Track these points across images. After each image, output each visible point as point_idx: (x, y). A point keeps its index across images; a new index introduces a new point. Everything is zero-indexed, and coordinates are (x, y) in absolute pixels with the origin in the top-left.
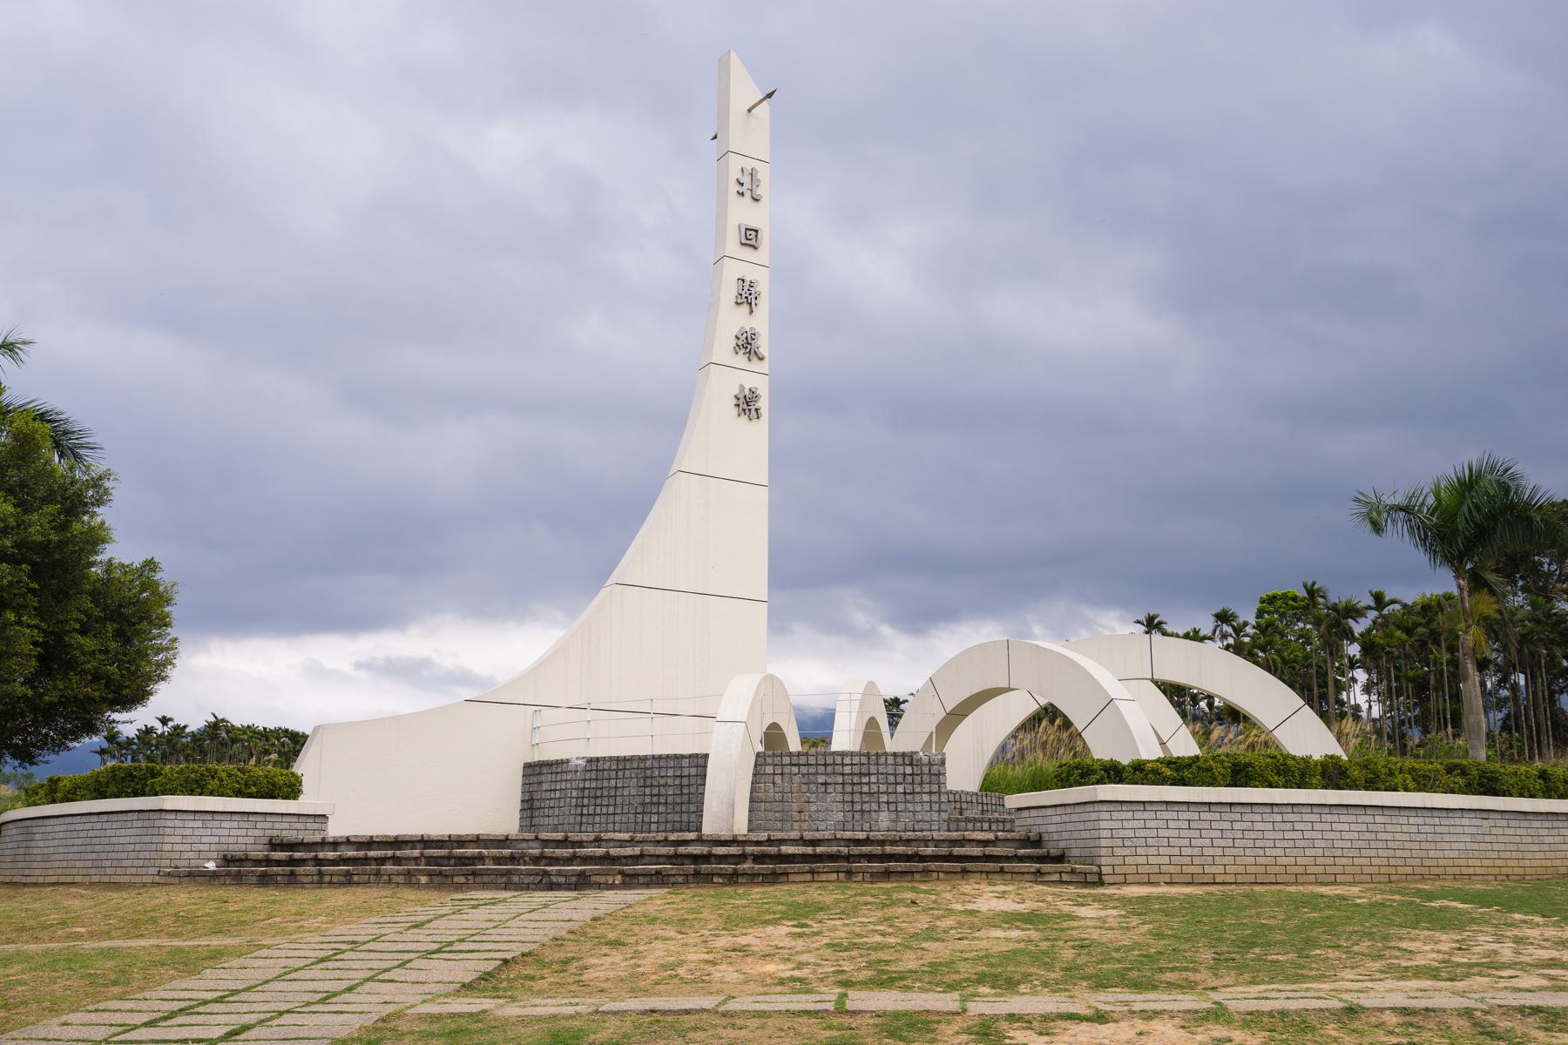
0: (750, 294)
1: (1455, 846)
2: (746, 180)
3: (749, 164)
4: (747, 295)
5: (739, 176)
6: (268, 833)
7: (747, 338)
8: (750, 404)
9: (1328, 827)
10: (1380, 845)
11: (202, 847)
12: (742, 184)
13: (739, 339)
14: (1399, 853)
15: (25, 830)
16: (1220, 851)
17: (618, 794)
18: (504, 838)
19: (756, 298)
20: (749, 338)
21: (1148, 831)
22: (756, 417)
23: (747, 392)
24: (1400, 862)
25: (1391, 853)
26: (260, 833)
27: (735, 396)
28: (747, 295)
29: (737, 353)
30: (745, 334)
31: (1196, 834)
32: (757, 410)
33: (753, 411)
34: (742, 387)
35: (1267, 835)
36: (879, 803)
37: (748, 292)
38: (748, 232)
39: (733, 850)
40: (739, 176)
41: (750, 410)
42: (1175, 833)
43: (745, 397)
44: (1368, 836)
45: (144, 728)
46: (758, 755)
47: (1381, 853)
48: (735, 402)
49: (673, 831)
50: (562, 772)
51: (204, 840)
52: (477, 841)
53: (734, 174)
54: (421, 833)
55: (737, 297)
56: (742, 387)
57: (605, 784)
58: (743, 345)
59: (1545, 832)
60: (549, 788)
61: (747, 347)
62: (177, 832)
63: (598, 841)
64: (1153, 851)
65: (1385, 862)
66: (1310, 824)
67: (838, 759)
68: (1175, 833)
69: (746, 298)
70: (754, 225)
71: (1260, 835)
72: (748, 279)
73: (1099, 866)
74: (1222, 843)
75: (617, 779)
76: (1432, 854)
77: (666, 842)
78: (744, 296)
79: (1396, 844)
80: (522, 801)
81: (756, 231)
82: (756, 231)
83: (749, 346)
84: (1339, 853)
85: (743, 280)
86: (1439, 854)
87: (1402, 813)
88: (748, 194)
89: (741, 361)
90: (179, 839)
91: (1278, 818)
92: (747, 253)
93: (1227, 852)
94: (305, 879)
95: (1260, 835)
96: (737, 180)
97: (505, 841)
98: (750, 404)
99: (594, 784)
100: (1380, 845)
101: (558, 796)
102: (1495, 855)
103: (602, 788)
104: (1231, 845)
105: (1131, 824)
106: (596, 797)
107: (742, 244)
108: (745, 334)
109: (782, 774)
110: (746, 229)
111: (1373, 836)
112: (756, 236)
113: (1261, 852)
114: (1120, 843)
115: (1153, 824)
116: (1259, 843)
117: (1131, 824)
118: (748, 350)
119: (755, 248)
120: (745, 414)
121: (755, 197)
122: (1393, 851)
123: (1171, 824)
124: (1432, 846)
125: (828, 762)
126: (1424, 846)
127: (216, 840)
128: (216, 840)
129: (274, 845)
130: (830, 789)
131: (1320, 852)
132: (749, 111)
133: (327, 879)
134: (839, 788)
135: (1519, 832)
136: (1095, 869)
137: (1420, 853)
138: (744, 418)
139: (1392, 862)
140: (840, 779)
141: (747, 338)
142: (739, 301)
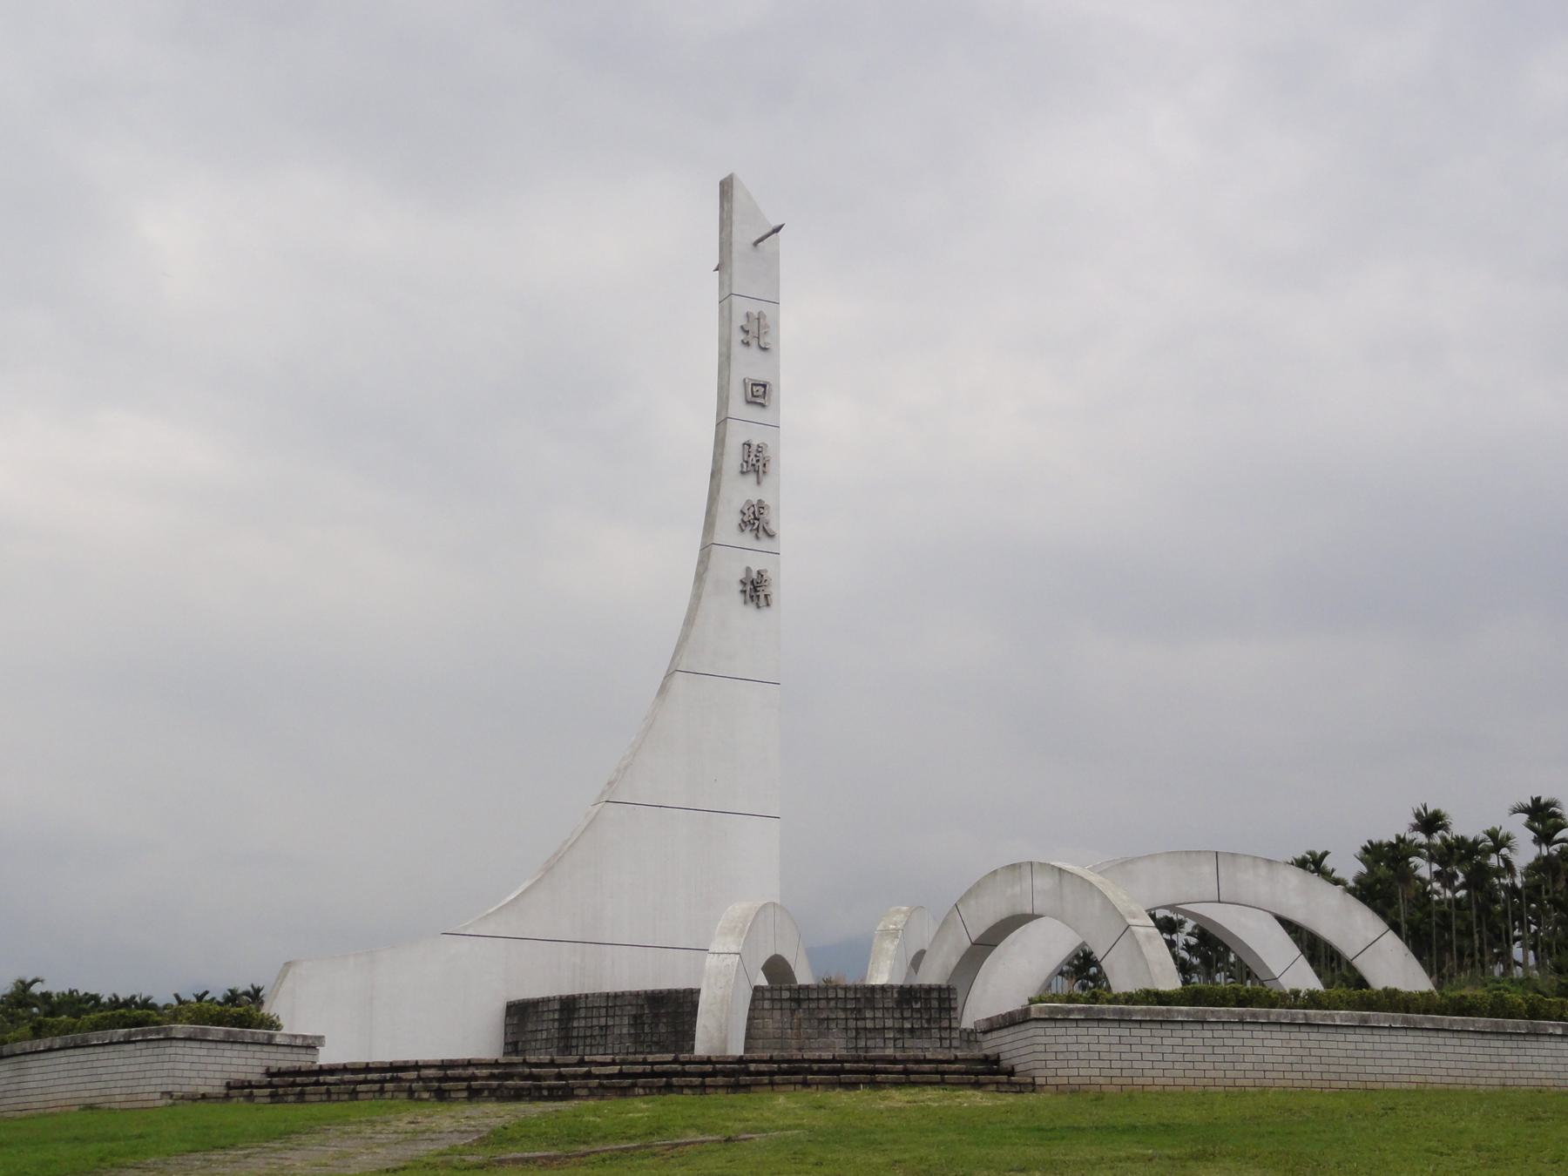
0: (758, 461)
1: (1397, 1063)
2: (753, 328)
3: (754, 308)
4: (754, 462)
5: (743, 322)
6: (266, 1063)
7: (754, 513)
8: (758, 589)
9: (1259, 1043)
10: (1313, 1060)
11: (207, 1074)
12: (747, 332)
13: (744, 514)
14: (1333, 1068)
15: (17, 1066)
16: (1149, 1065)
17: (608, 1033)
18: (493, 1062)
19: (765, 465)
20: (756, 513)
21: (1081, 1046)
22: (765, 604)
23: (754, 576)
24: (1333, 1076)
25: (1325, 1068)
26: (256, 1062)
27: (741, 581)
28: (754, 462)
29: (743, 531)
30: (752, 509)
31: (1126, 1048)
32: (766, 596)
33: (762, 597)
34: (748, 570)
35: (1197, 1050)
36: (885, 1039)
37: (755, 459)
38: (755, 389)
39: (709, 1068)
40: (743, 322)
41: (758, 596)
42: (1106, 1048)
43: (752, 582)
44: (1301, 1052)
45: (1402, 836)
46: (757, 989)
47: (1314, 1068)
48: (740, 587)
49: (651, 1053)
50: (549, 1011)
51: (210, 1067)
52: (469, 1064)
53: (739, 320)
54: (415, 1059)
55: (742, 465)
56: (748, 570)
57: (595, 1022)
58: (749, 521)
59: (1507, 1052)
60: (534, 1029)
61: (754, 524)
62: (187, 1058)
63: (581, 1063)
64: (1084, 1064)
65: (1318, 1076)
66: (1215, 1036)
67: (841, 994)
68: (1106, 1048)
69: (753, 465)
70: (761, 378)
71: (1190, 1050)
72: (755, 443)
73: (1034, 1078)
74: (1152, 1057)
75: (607, 1017)
76: (1369, 1070)
77: (645, 1062)
78: (750, 463)
79: (1331, 1060)
80: (506, 1044)
81: (764, 386)
82: (764, 386)
83: (756, 521)
84: (1269, 1067)
85: (749, 445)
86: (1378, 1070)
87: (1339, 1030)
88: (754, 343)
89: (747, 539)
90: (187, 1066)
91: (1209, 1034)
92: (753, 413)
93: (1156, 1065)
94: (312, 1098)
95: (1190, 1050)
96: (742, 327)
97: (496, 1064)
98: (758, 589)
99: (584, 1022)
100: (1313, 1060)
101: (544, 1037)
102: (1444, 1072)
103: (592, 1027)
104: (1161, 1058)
105: (1063, 1040)
106: (585, 1037)
107: (748, 402)
108: (752, 509)
109: (781, 1009)
110: (753, 385)
111: (1306, 1052)
112: (765, 392)
113: (1190, 1066)
114: (1052, 1056)
115: (1086, 1040)
116: (1188, 1058)
117: (1063, 1040)
118: (756, 526)
119: (763, 405)
120: (753, 601)
121: (763, 346)
122: (1327, 1066)
123: (1102, 1040)
124: (1371, 1062)
125: (830, 997)
126: (1361, 1062)
127: (219, 1067)
128: (219, 1067)
129: (269, 1073)
130: (833, 1025)
131: (1250, 1066)
132: (756, 243)
133: (334, 1097)
134: (842, 1024)
135: (1474, 1050)
136: (1029, 1080)
137: (1358, 1069)
138: (751, 608)
139: (1325, 1076)
140: (841, 1015)
141: (754, 513)
142: (745, 470)
